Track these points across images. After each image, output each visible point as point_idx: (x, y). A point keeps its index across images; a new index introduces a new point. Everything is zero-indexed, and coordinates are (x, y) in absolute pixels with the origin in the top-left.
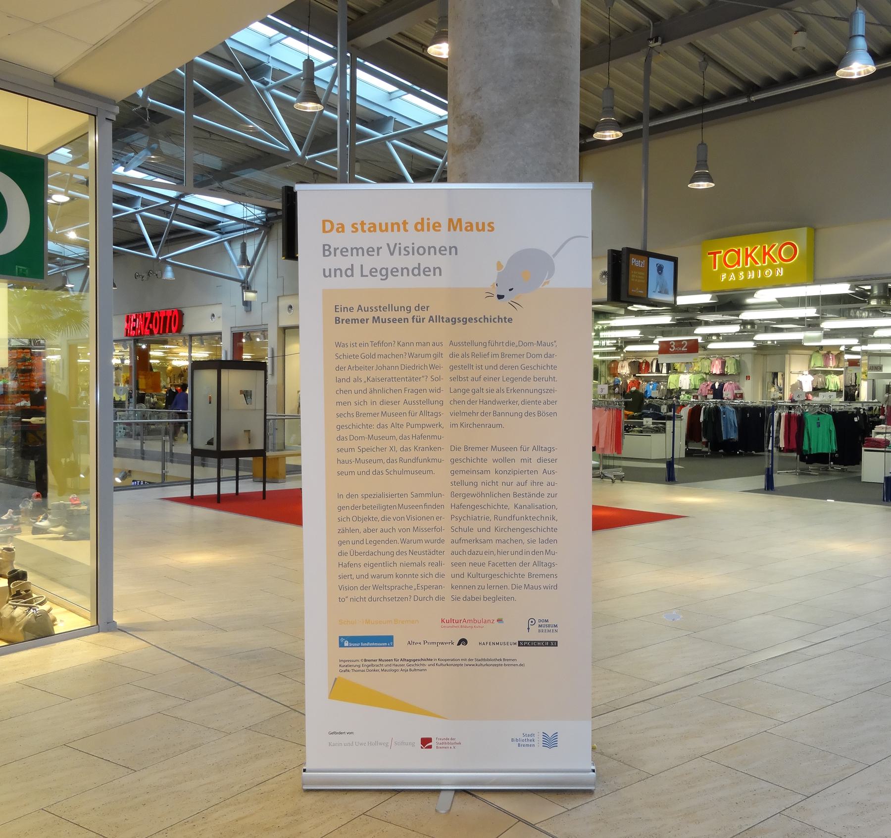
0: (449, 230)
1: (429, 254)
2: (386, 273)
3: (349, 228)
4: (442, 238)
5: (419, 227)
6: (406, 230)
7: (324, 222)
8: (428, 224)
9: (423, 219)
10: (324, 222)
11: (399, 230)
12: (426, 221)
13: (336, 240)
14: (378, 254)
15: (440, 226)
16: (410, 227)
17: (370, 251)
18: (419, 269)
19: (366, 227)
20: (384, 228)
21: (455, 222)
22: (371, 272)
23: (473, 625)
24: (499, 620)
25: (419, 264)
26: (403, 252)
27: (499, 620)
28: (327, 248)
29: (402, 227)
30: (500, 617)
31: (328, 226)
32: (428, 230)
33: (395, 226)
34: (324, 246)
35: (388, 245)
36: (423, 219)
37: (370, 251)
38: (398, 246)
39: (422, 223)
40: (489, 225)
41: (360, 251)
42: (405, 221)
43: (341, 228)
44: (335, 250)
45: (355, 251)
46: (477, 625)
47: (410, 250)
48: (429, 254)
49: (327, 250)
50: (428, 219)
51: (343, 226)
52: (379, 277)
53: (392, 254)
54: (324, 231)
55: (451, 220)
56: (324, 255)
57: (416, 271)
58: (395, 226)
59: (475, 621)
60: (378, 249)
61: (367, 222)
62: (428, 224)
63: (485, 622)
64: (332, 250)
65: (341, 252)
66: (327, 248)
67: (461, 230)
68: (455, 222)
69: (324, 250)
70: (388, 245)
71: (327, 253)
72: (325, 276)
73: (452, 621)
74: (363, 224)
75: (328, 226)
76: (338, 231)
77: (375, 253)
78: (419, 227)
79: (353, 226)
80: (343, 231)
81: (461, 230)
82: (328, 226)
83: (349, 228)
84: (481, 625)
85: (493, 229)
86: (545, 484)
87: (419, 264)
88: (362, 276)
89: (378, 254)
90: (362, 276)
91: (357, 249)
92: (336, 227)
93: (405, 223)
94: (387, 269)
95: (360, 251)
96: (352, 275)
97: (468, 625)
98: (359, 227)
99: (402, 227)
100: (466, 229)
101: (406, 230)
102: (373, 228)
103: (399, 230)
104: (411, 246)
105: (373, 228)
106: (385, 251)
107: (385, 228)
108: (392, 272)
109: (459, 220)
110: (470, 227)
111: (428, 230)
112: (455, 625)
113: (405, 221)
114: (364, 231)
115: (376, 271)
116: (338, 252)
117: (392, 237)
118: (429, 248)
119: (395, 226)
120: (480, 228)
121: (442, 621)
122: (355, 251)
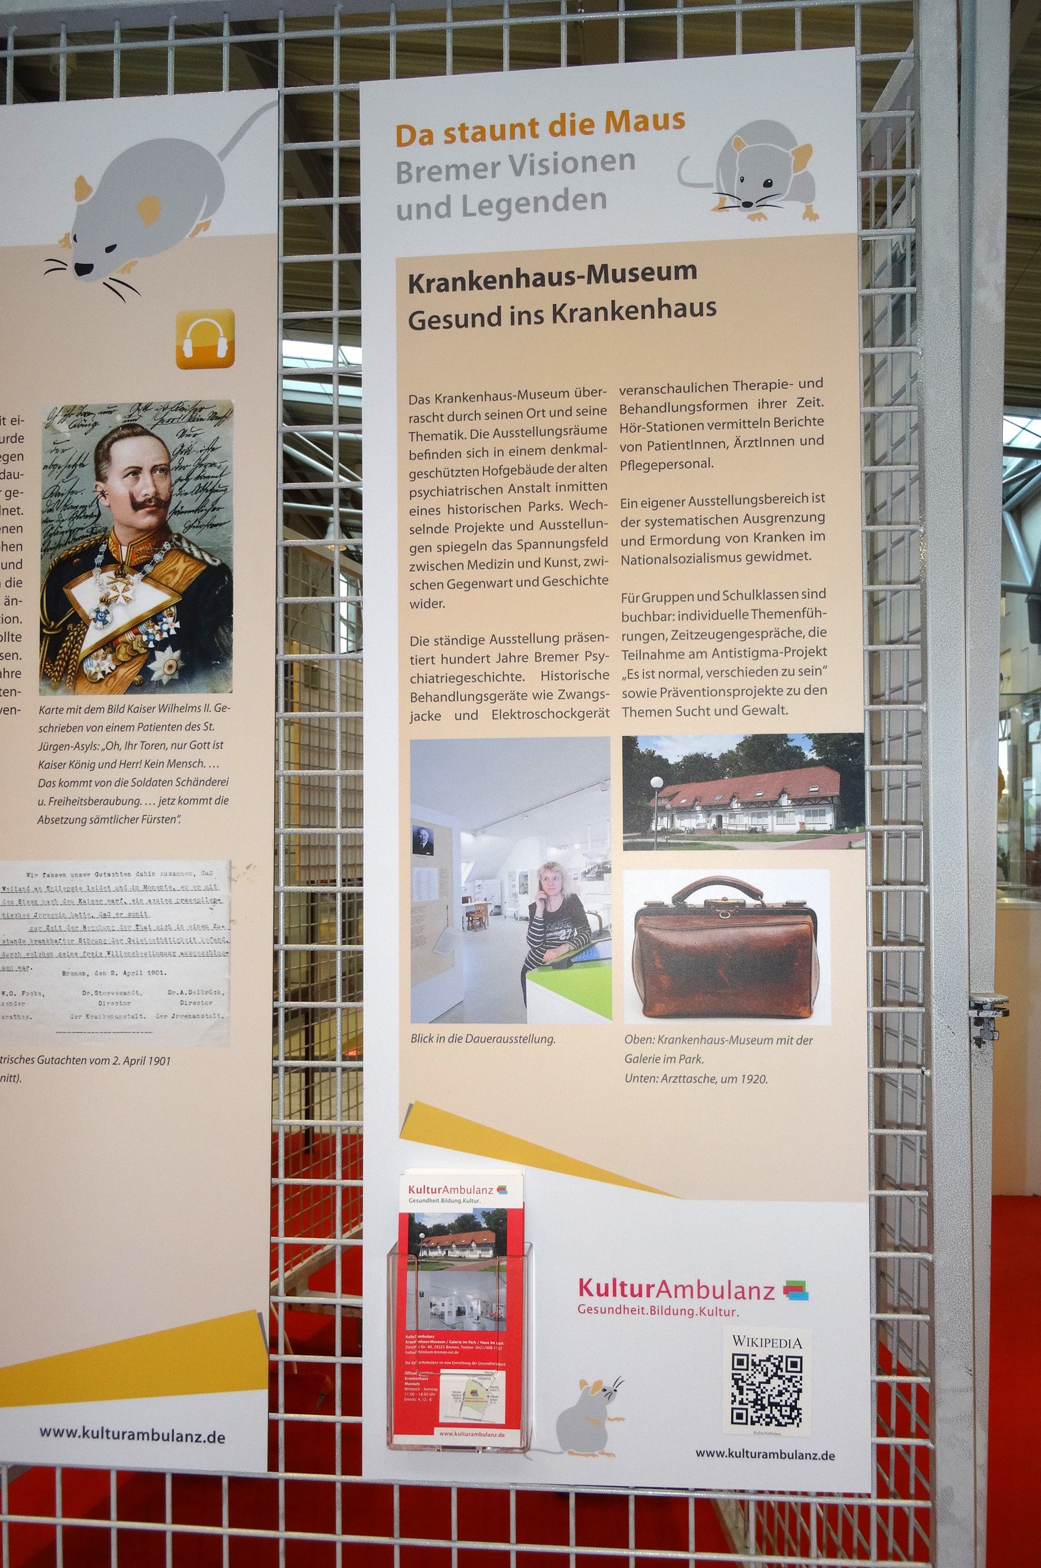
0: (608, 131)
1: (584, 170)
2: (507, 209)
3: (439, 137)
4: (602, 143)
5: (557, 129)
6: (535, 135)
7: (400, 128)
8: (573, 122)
9: (563, 116)
10: (400, 128)
11: (523, 136)
12: (568, 119)
13: (417, 155)
14: (494, 176)
15: (592, 125)
16: (542, 129)
17: (479, 171)
18: (566, 198)
19: (468, 134)
20: (498, 133)
21: (618, 117)
22: (481, 207)
23: (695, 1304)
24: (795, 1290)
25: (566, 190)
26: (538, 169)
27: (795, 1290)
28: (404, 168)
29: (528, 129)
30: (796, 1277)
31: (407, 135)
32: (573, 133)
33: (517, 130)
34: (399, 164)
35: (511, 157)
36: (563, 116)
37: (479, 171)
38: (529, 158)
39: (562, 122)
40: (676, 117)
41: (462, 170)
42: (533, 120)
43: (428, 138)
44: (419, 170)
45: (453, 171)
46: (710, 1303)
47: (550, 164)
48: (584, 170)
49: (404, 173)
50: (573, 115)
51: (429, 134)
52: (496, 214)
53: (518, 173)
54: (400, 144)
55: (610, 115)
56: (400, 181)
57: (561, 203)
58: (517, 130)
59: (701, 1290)
60: (494, 166)
61: (470, 124)
62: (573, 122)
63: (741, 1295)
64: (413, 172)
65: (430, 173)
66: (404, 168)
67: (628, 129)
68: (618, 117)
69: (400, 172)
70: (511, 157)
71: (405, 177)
72: (401, 218)
73: (618, 1287)
74: (463, 128)
75: (406, 135)
76: (422, 142)
77: (489, 173)
78: (557, 129)
79: (447, 132)
80: (431, 142)
81: (628, 129)
82: (406, 135)
83: (439, 137)
84: (725, 1304)
85: (682, 124)
86: (133, 875)
87: (566, 190)
88: (466, 214)
89: (494, 176)
90: (466, 214)
91: (457, 168)
92: (419, 135)
93: (533, 123)
94: (509, 201)
95: (462, 170)
96: (448, 214)
97: (678, 1303)
98: (457, 133)
99: (528, 129)
100: (637, 128)
101: (535, 135)
102: (480, 134)
103: (523, 136)
104: (551, 157)
105: (480, 134)
106: (505, 170)
107: (498, 134)
108: (518, 205)
109: (625, 114)
110: (643, 124)
111: (573, 133)
112: (631, 1302)
113: (533, 120)
114: (464, 140)
115: (491, 206)
116: (424, 174)
117: (519, 147)
118: (584, 159)
119: (518, 130)
120: (661, 123)
121: (583, 1287)
122: (453, 171)
